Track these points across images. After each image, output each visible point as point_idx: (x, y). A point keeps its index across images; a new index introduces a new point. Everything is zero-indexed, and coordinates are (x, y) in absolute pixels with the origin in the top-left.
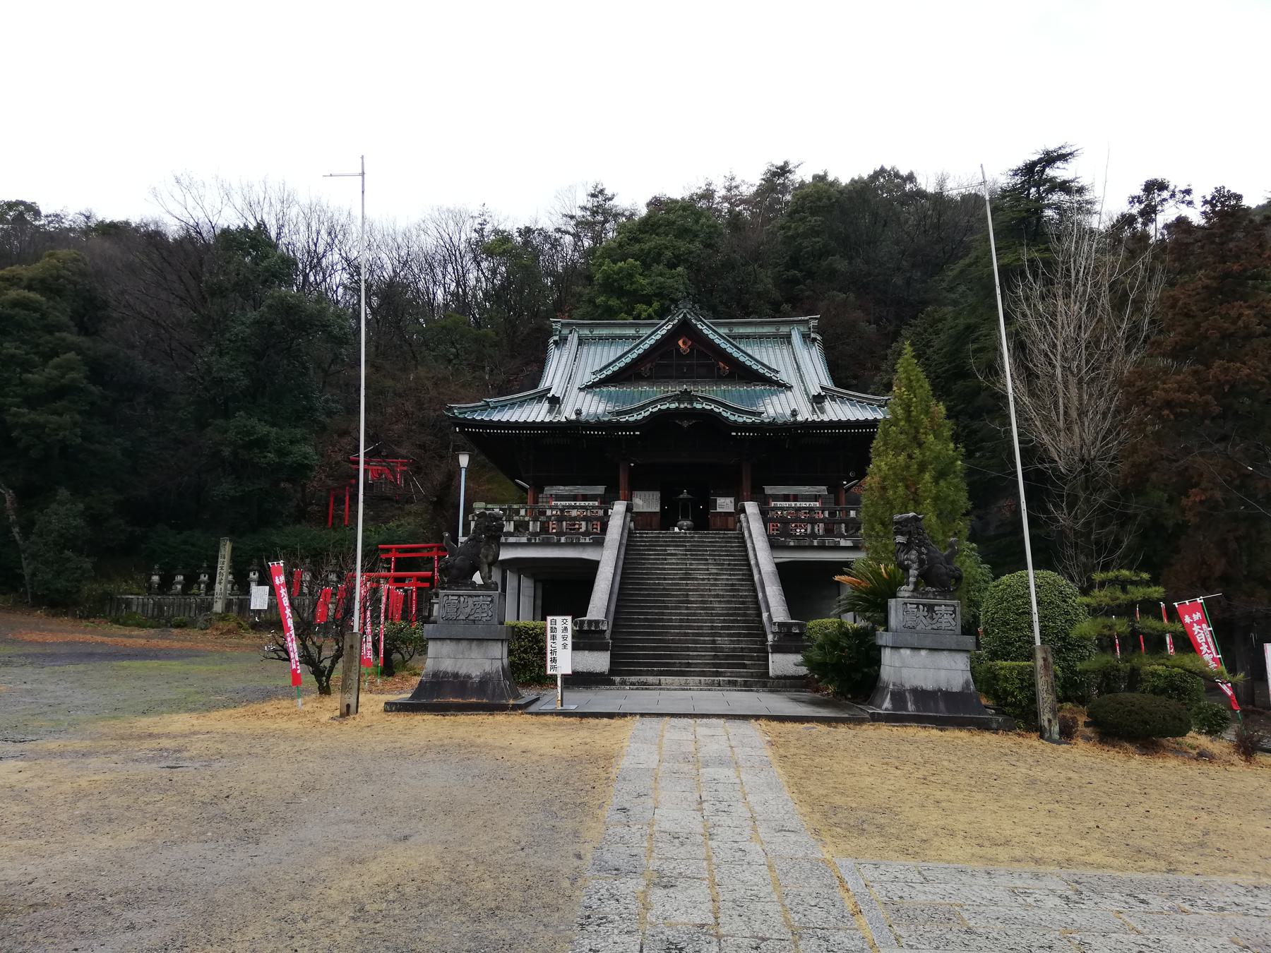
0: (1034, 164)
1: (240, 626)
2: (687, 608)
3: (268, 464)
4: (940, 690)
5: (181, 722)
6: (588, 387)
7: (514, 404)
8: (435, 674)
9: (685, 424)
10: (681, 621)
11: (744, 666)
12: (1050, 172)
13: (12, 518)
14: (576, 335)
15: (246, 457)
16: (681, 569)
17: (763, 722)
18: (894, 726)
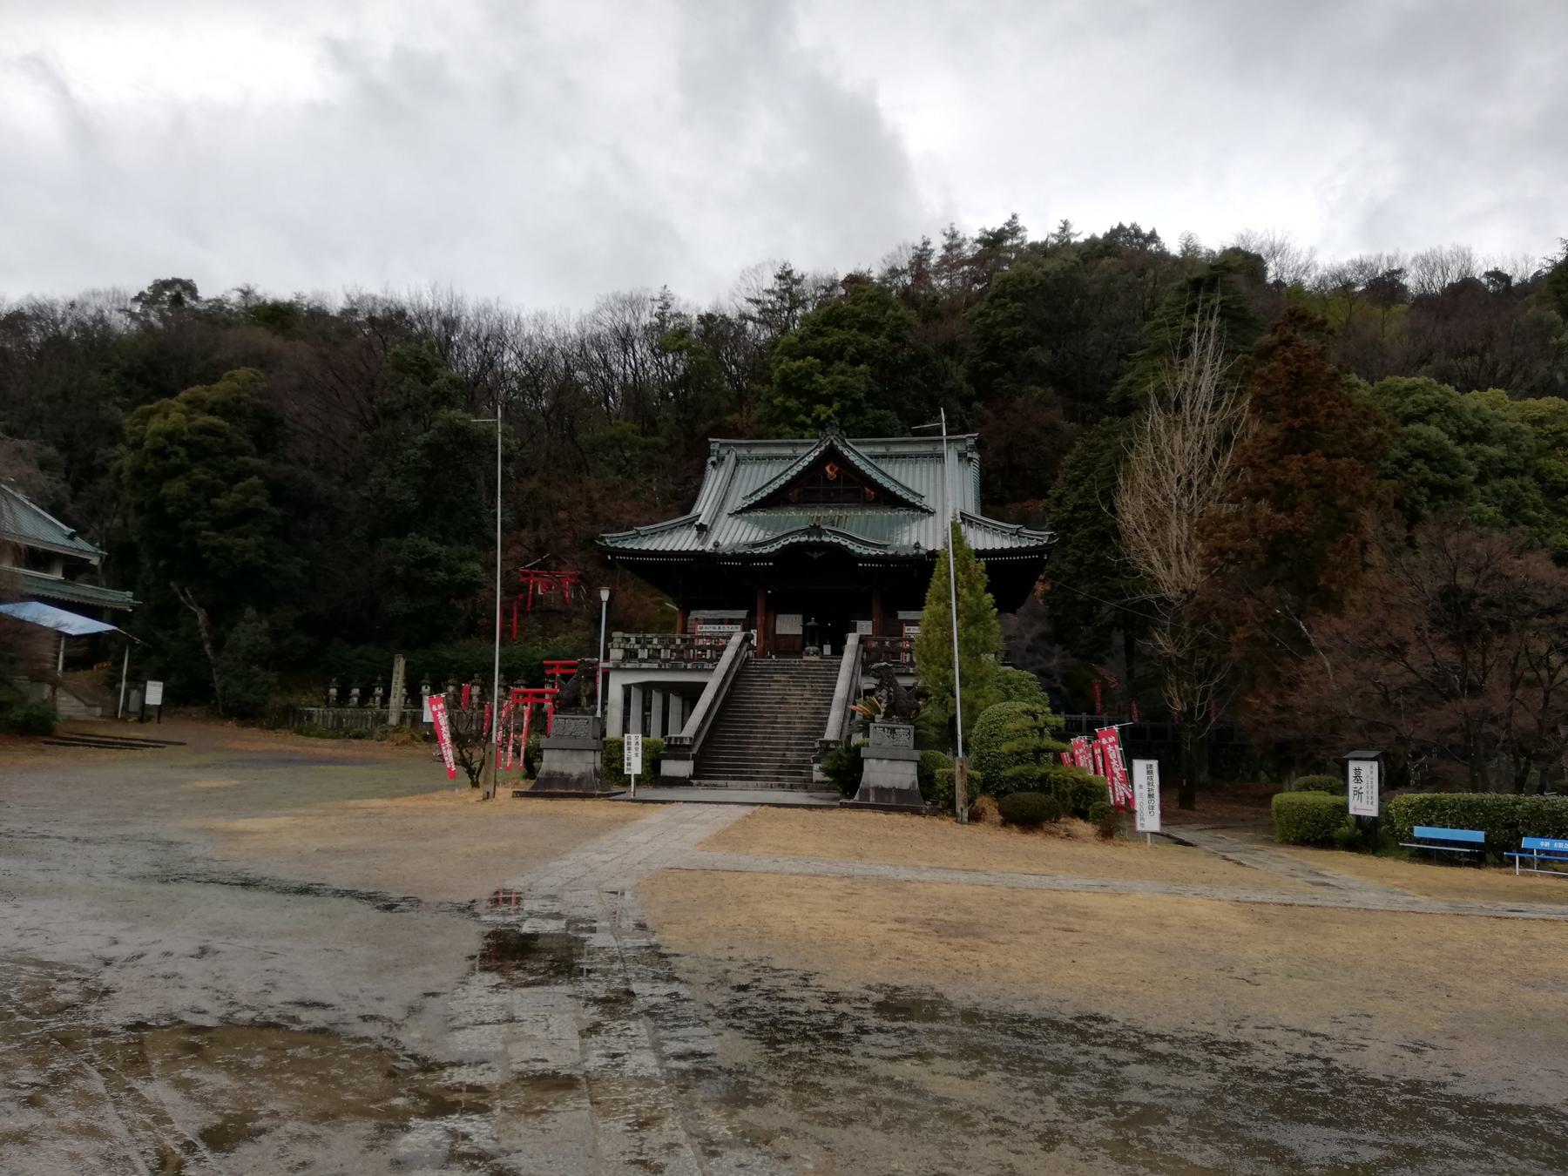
1: (413, 738)
3: (439, 582)
5: (378, 803)
6: (744, 510)
9: (816, 555)
11: (801, 774)
13: (204, 635)
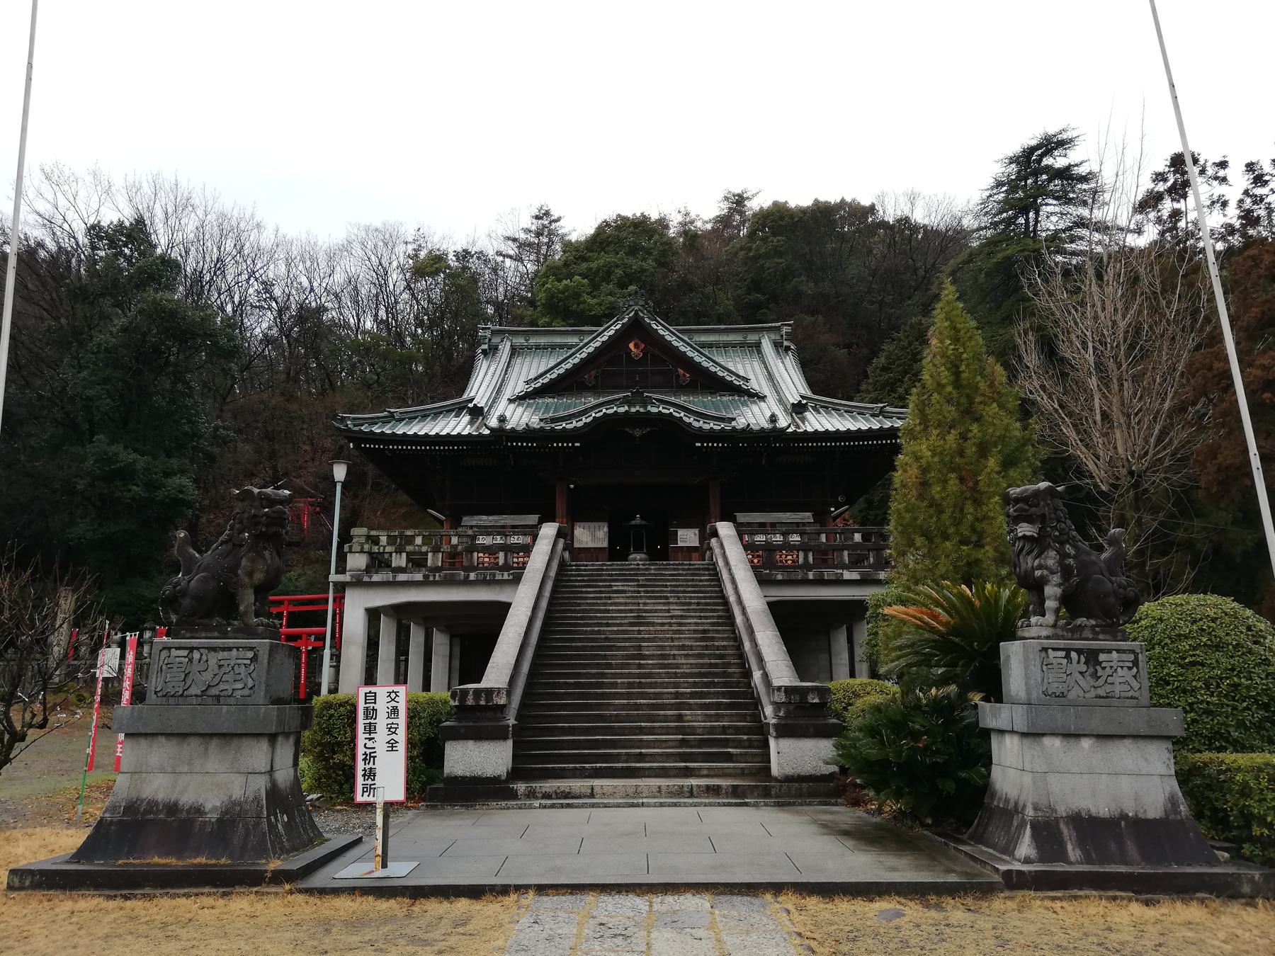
0: (1032, 150)
2: (640, 666)
3: (133, 499)
4: (1124, 816)
7: (425, 416)
8: (131, 807)
9: (638, 433)
10: (630, 685)
11: (729, 757)
12: (1047, 161)
14: (509, 344)
15: (105, 491)
16: (631, 611)
17: (789, 900)
18: (1054, 899)
